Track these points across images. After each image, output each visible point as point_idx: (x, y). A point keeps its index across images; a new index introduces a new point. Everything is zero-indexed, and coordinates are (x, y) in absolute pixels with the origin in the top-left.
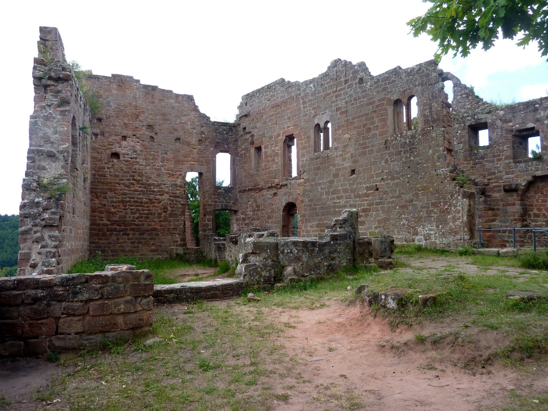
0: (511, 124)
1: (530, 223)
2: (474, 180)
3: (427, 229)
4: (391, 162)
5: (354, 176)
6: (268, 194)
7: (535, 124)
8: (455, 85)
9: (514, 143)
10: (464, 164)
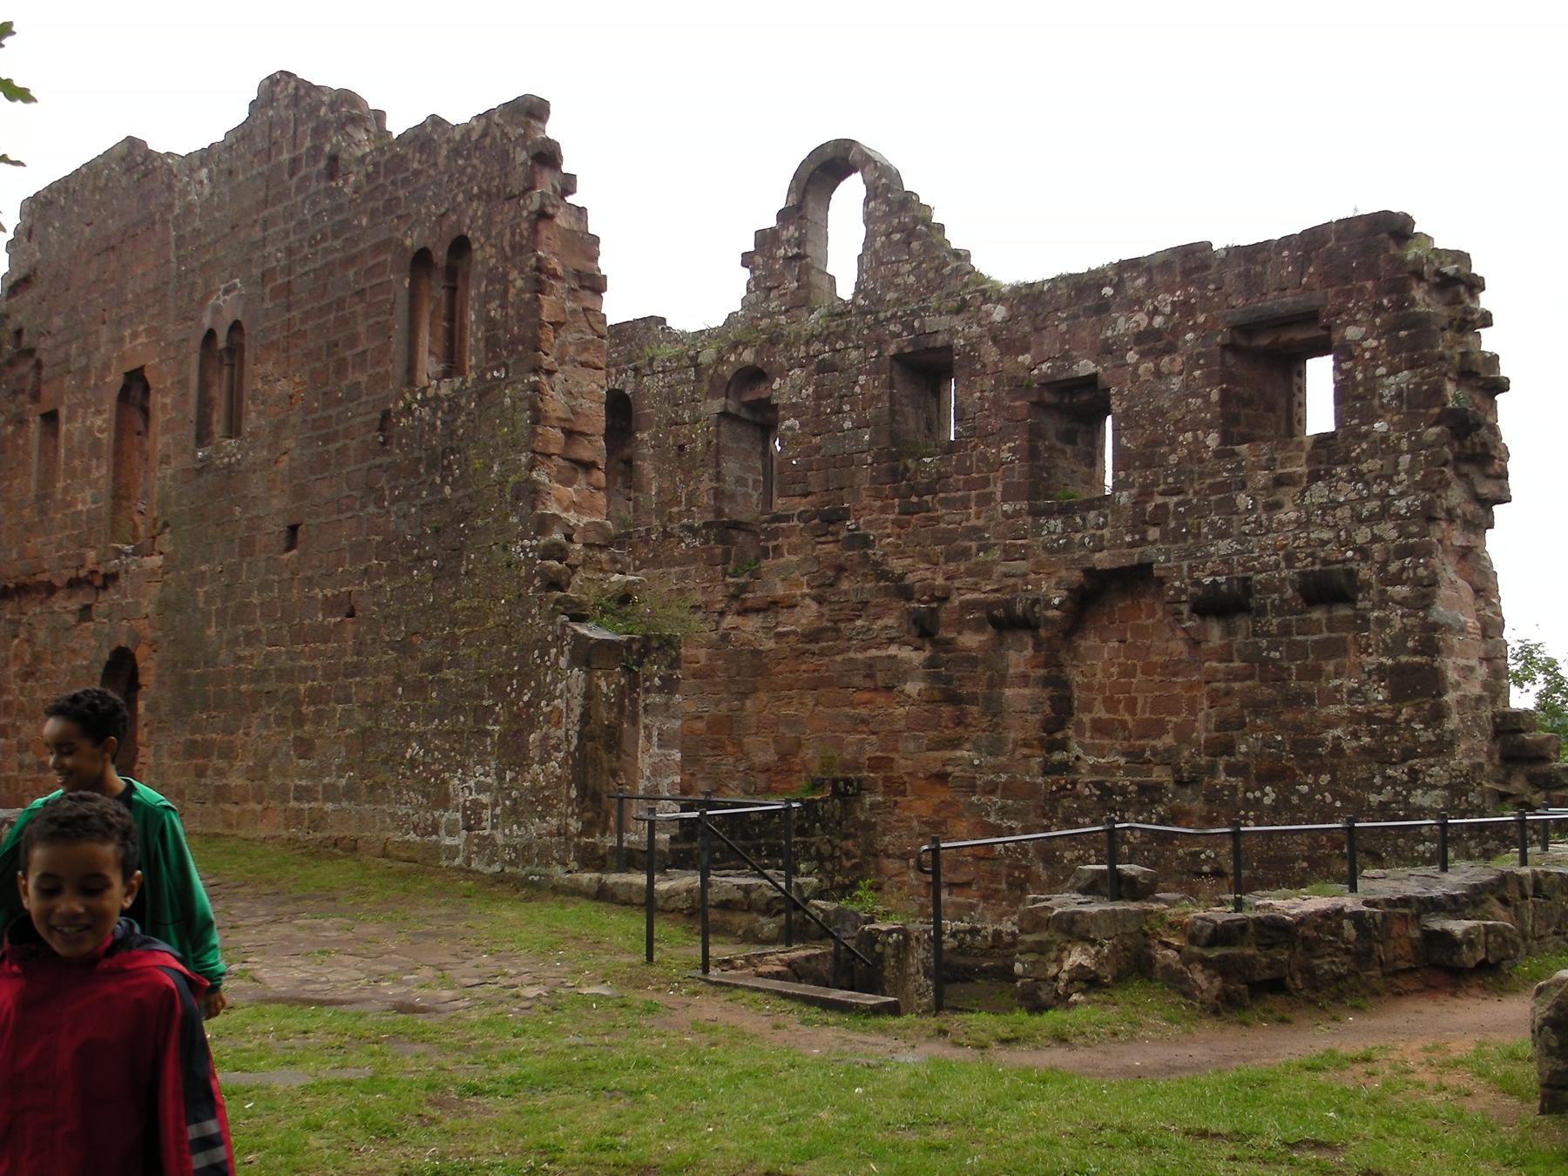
0: (1026, 359)
1: (1078, 758)
2: (902, 577)
3: (472, 783)
4: (393, 502)
5: (294, 552)
6: (66, 605)
7: (1097, 363)
8: (873, 193)
9: (1035, 433)
10: (872, 511)
